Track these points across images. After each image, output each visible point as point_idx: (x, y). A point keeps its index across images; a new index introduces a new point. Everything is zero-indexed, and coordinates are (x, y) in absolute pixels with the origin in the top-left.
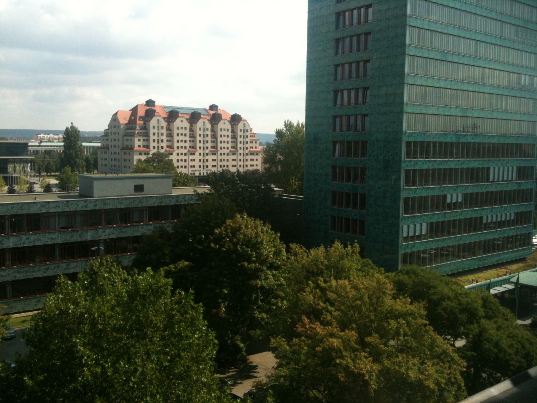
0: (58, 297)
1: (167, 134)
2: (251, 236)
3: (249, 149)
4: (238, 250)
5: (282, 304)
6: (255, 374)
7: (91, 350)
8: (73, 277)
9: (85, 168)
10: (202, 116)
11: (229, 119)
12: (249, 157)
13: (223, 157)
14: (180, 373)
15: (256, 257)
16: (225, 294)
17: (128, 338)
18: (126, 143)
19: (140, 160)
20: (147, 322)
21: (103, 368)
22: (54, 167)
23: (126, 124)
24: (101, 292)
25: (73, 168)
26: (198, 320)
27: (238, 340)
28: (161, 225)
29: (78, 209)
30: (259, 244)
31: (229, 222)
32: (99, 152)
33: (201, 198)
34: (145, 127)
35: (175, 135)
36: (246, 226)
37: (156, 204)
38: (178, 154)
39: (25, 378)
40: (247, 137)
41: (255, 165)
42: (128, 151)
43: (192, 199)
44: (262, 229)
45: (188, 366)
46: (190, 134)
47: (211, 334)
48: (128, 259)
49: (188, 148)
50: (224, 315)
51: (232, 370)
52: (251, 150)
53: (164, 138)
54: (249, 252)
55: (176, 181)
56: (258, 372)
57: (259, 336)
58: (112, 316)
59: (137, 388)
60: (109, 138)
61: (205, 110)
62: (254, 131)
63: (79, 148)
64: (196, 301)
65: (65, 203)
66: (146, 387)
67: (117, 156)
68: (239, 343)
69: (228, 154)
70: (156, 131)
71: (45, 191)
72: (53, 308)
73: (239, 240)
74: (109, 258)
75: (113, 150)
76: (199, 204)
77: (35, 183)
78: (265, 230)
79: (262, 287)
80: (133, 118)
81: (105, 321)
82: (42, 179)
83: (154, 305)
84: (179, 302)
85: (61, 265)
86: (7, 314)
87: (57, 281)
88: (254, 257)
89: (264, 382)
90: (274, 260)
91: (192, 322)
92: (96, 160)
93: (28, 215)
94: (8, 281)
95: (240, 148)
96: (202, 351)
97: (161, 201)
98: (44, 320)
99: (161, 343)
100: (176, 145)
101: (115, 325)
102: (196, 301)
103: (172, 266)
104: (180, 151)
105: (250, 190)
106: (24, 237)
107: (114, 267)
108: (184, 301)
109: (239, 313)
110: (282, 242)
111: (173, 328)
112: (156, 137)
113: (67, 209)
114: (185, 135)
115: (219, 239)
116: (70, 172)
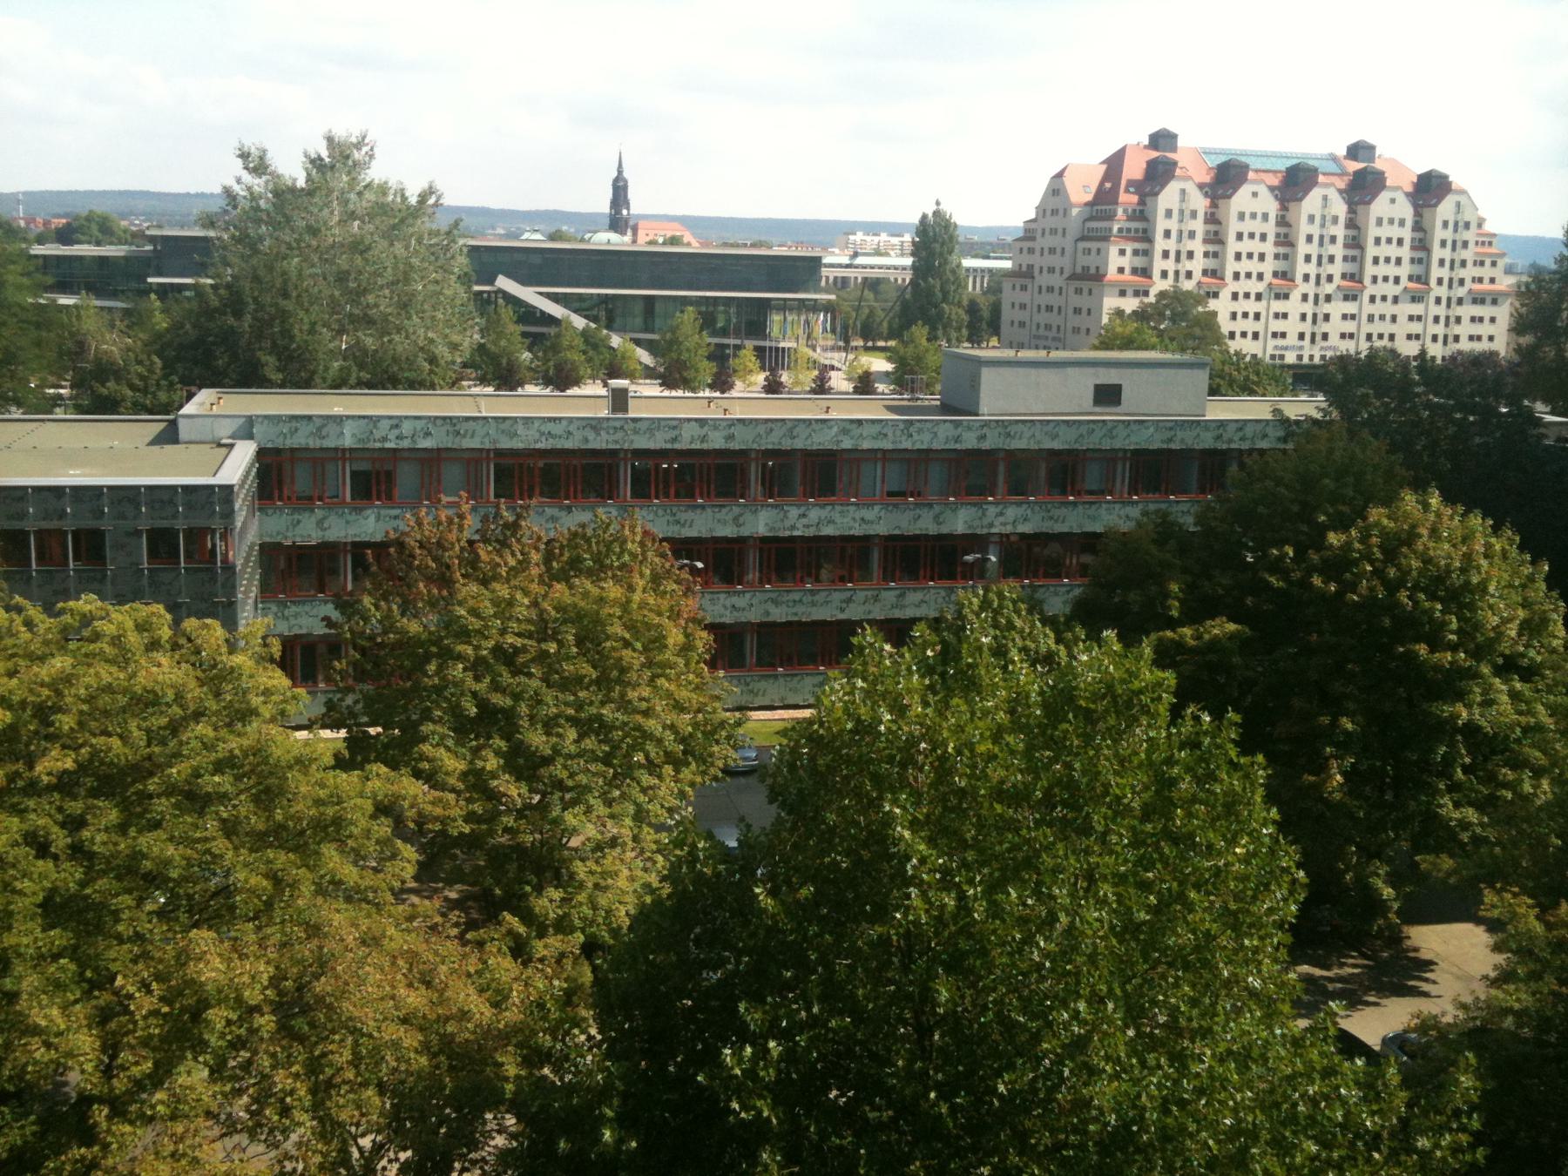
0: (854, 687)
1: (1207, 232)
2: (1448, 565)
3: (1468, 284)
4: (1398, 604)
5: (1535, 787)
6: (1425, 987)
7: (931, 842)
8: (897, 631)
9: (965, 332)
10: (1321, 179)
11: (1409, 189)
12: (1467, 311)
13: (1378, 308)
14: (1182, 948)
15: (1458, 632)
16: (1346, 732)
17: (1038, 823)
18: (1083, 261)
19: (1119, 313)
20: (1093, 788)
21: (961, 897)
22: (885, 324)
23: (1086, 204)
24: (970, 684)
25: (933, 328)
26: (1249, 804)
27: (1378, 875)
28: (1163, 506)
29: (936, 446)
30: (1472, 592)
31: (1376, 514)
32: (1006, 285)
33: (1293, 434)
34: (1142, 212)
35: (1231, 238)
36: (1434, 533)
37: (1156, 445)
38: (1235, 296)
39: (757, 890)
40: (1465, 244)
41: (1485, 339)
42: (1085, 285)
43: (1265, 436)
44: (1488, 546)
45: (1207, 934)
46: (1278, 235)
47: (1287, 853)
48: (1060, 597)
49: (1268, 277)
50: (1337, 796)
51: (1351, 961)
52: (1477, 287)
53: (1198, 246)
54: (1438, 614)
55: (1222, 378)
56: (1434, 982)
57: (1449, 874)
58: (996, 757)
59: (1052, 970)
60: (1037, 245)
61: (1334, 158)
62: (1489, 227)
63: (953, 272)
64: (1246, 747)
65: (902, 426)
66: (1077, 974)
67: (1053, 299)
68: (1380, 884)
69: (1396, 300)
70: (1173, 225)
71: (857, 390)
72: (840, 714)
73: (1405, 573)
74: (1010, 589)
75: (1044, 280)
76: (1284, 451)
77: (833, 368)
78: (1498, 547)
79: (1471, 730)
80: (1108, 185)
81: (974, 767)
82: (851, 356)
83: (1115, 741)
84: (1193, 744)
85: (884, 594)
86: (740, 709)
87: (855, 640)
88: (1452, 632)
89: (1448, 1019)
90: (1522, 649)
91: (1231, 806)
92: (996, 310)
93: (807, 454)
94: (749, 623)
95: (1440, 281)
96: (1254, 898)
97: (1169, 434)
98: (814, 740)
99: (1130, 855)
100: (1231, 266)
101: (1002, 782)
102: (1246, 747)
103: (1187, 631)
104: (1243, 286)
105: (1458, 416)
106: (794, 512)
107: (1019, 616)
108: (1207, 741)
109: (1388, 797)
110: (1554, 594)
111: (1170, 818)
112: (1171, 245)
113: (907, 444)
114: (1263, 237)
115: (1338, 566)
116: (924, 342)
